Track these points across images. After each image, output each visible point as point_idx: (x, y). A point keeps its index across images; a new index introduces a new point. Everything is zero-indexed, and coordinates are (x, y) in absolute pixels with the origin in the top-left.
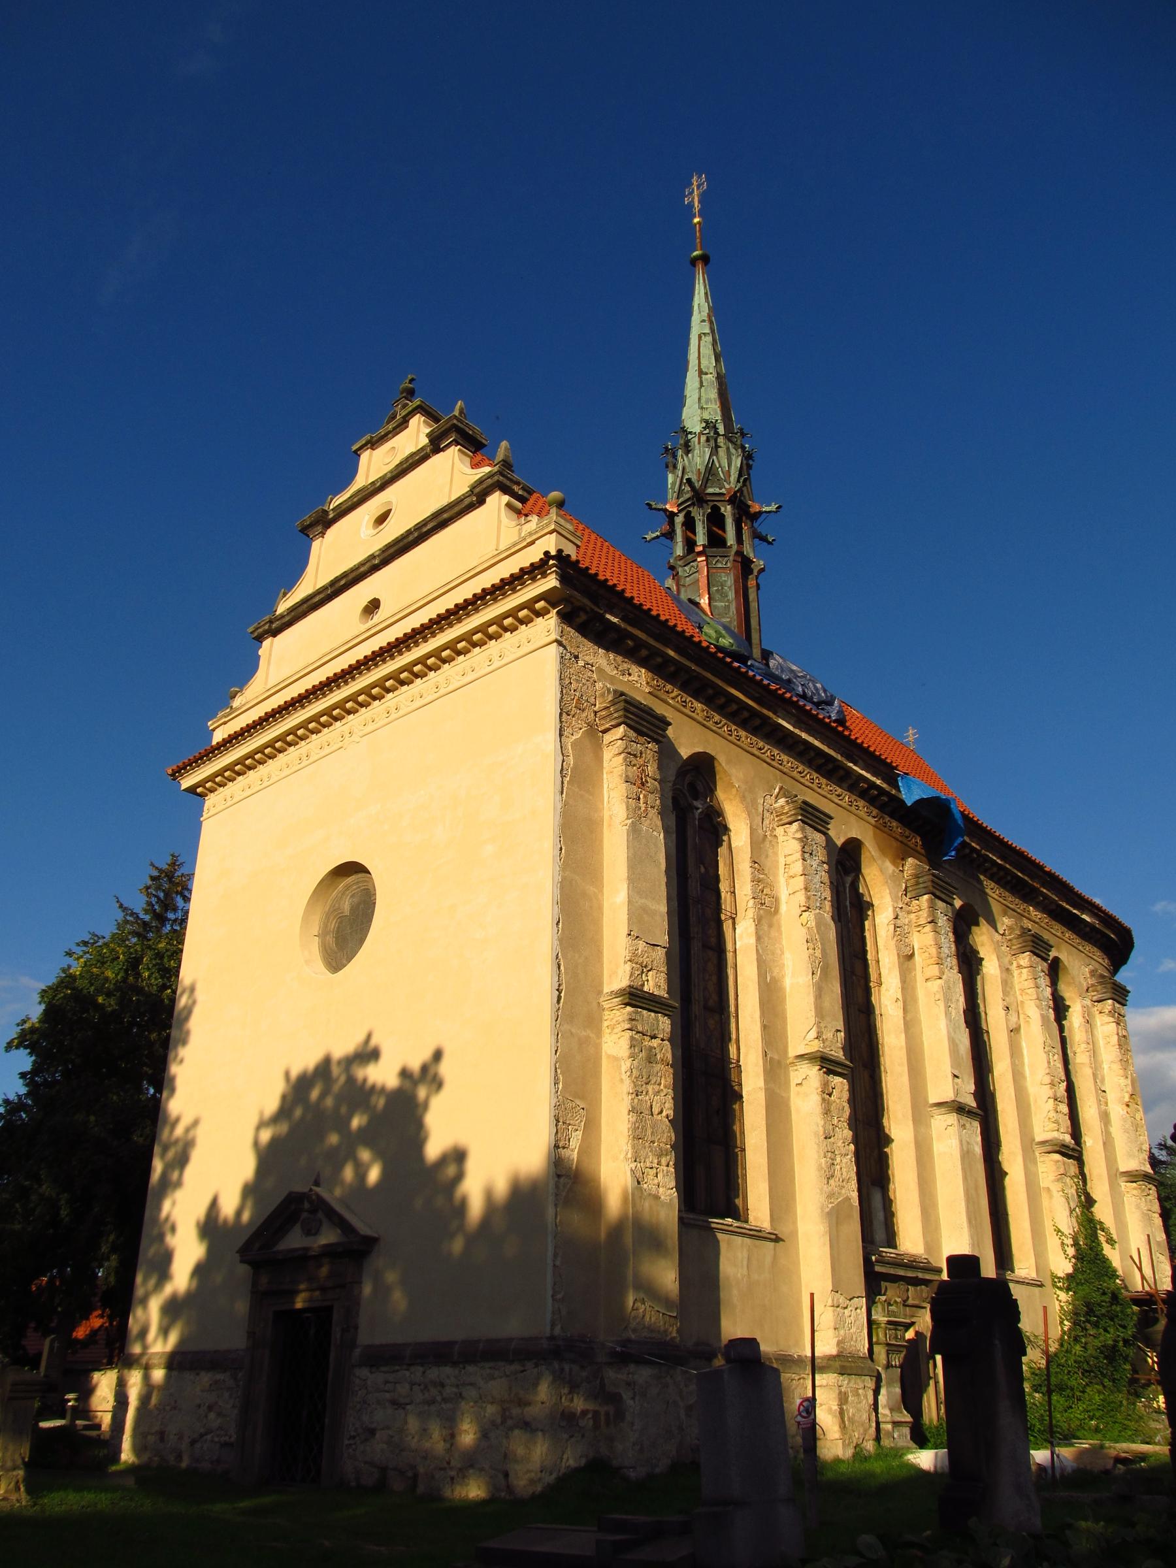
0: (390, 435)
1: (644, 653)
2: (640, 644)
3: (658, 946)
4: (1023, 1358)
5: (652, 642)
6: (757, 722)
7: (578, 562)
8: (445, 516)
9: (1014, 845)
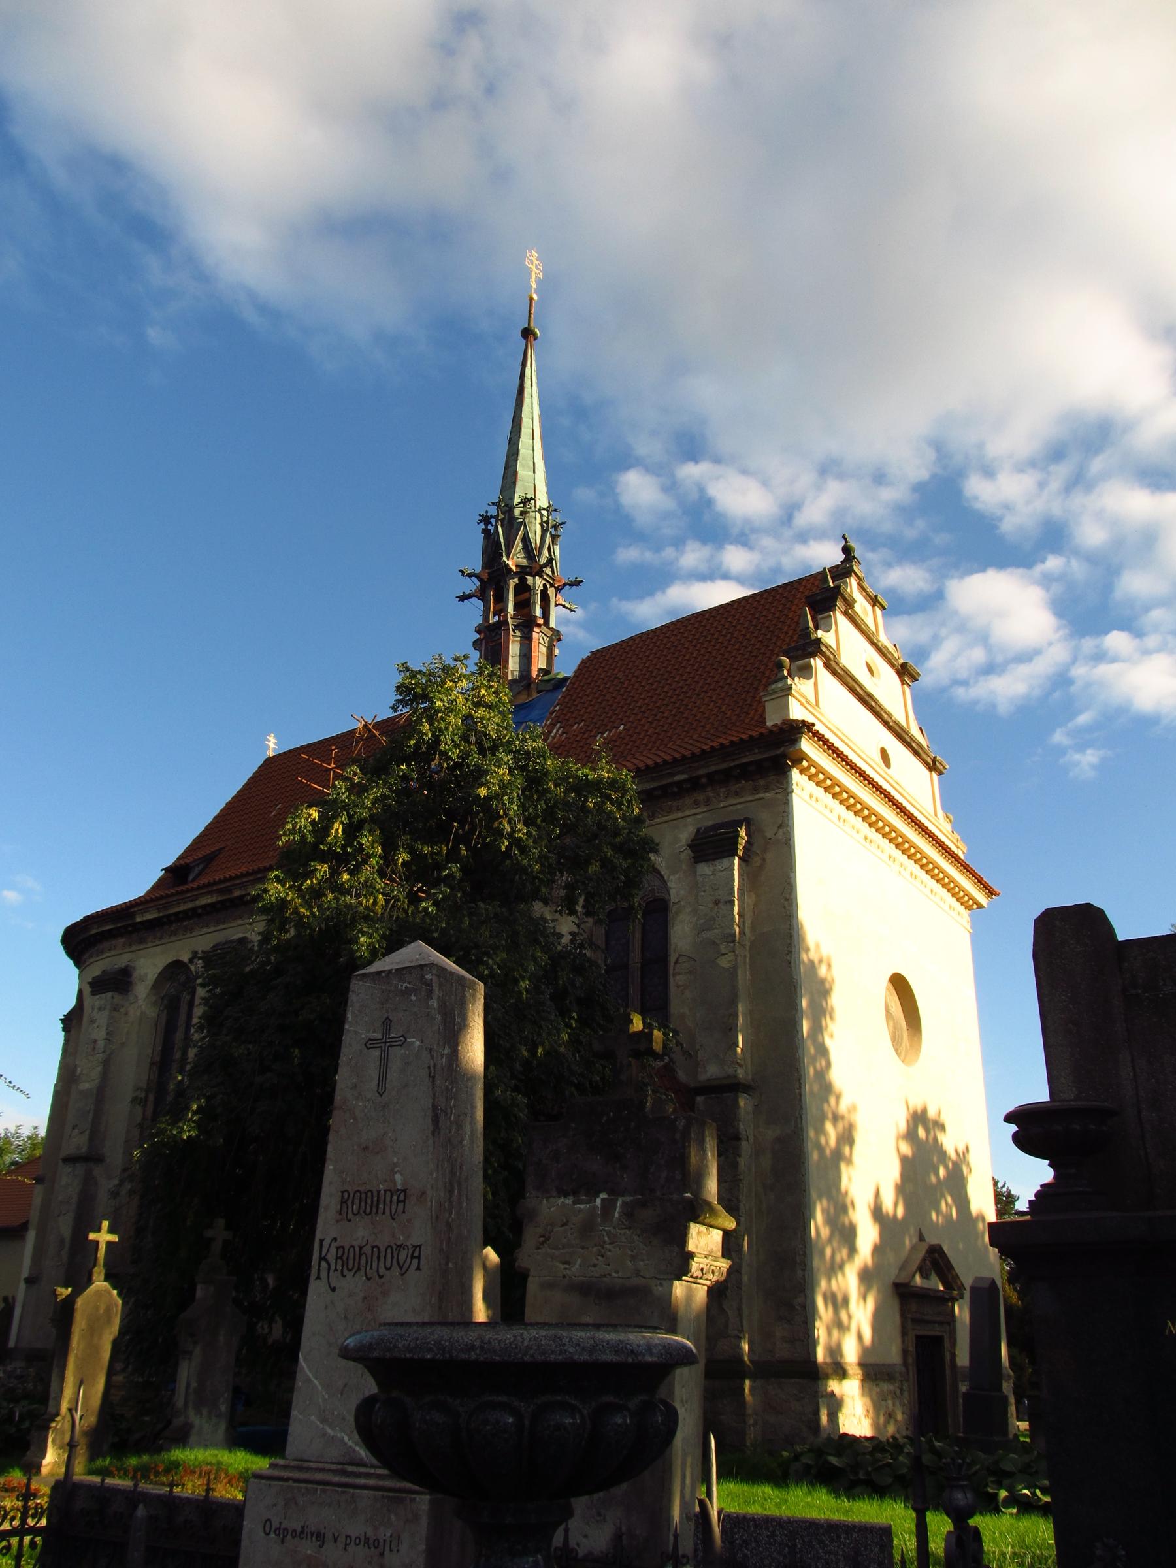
0: (864, 593)
8: (920, 751)
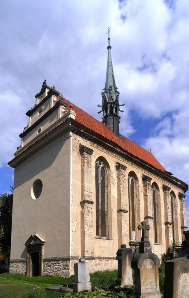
1: (89, 137)
2: (88, 136)
3: (108, 209)
4: (127, 247)
5: (91, 135)
6: (113, 150)
7: (76, 121)
9: (121, 146)
